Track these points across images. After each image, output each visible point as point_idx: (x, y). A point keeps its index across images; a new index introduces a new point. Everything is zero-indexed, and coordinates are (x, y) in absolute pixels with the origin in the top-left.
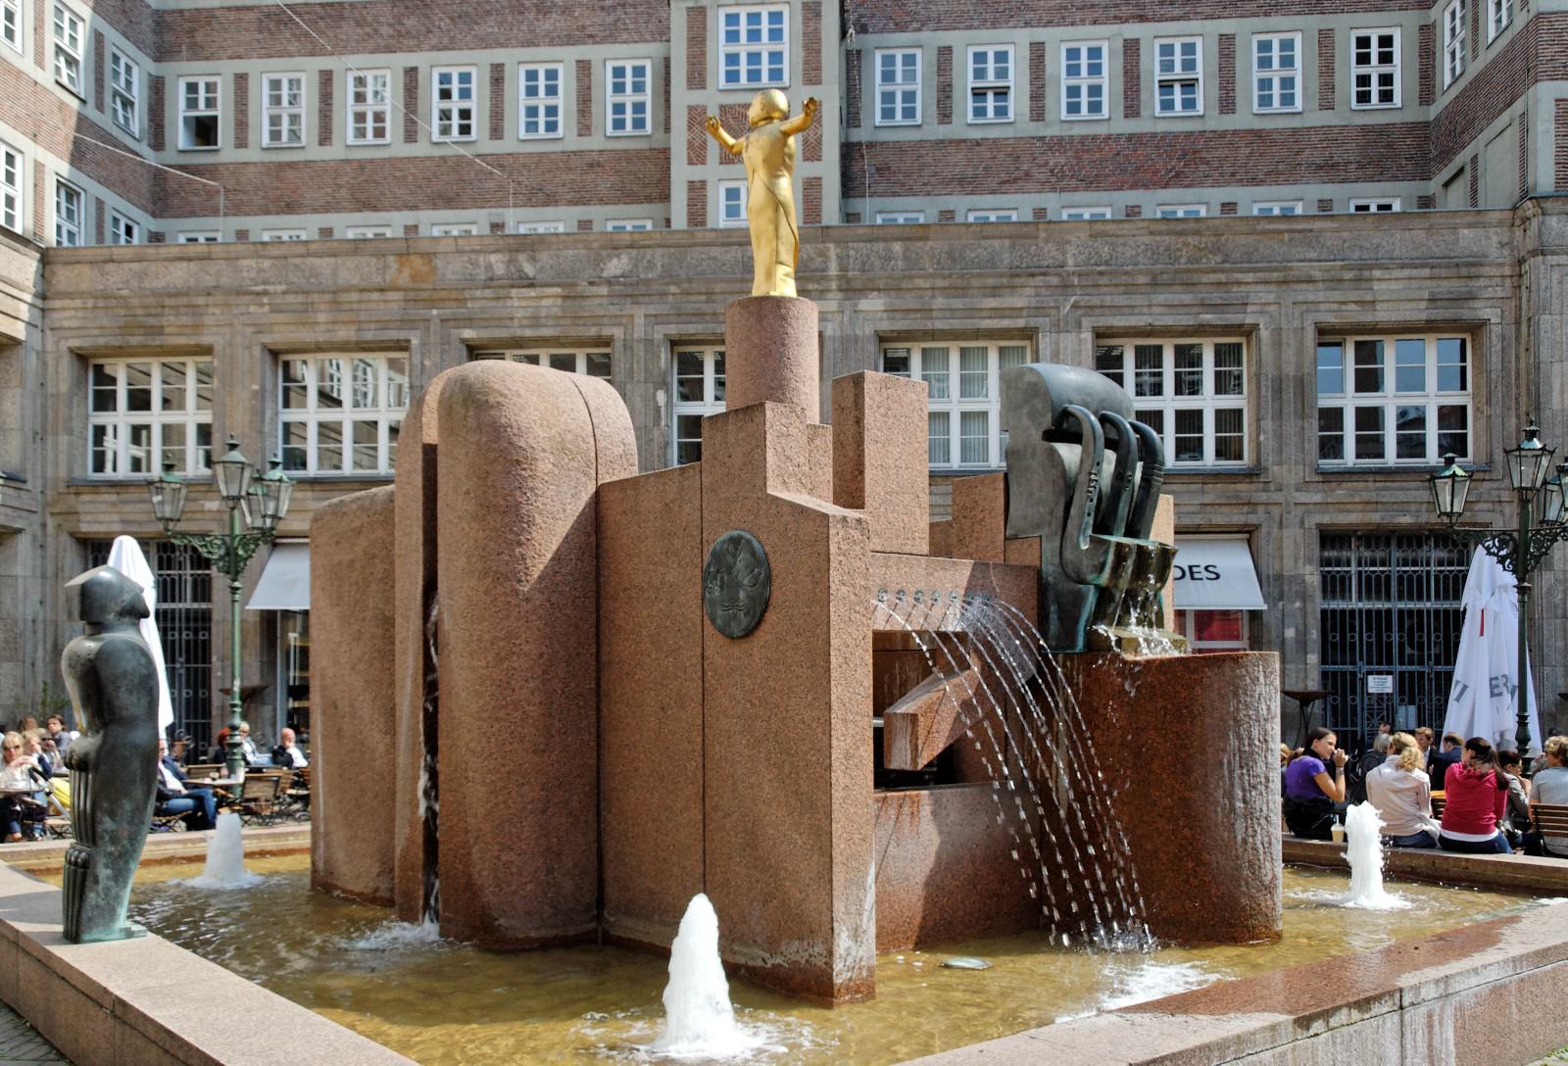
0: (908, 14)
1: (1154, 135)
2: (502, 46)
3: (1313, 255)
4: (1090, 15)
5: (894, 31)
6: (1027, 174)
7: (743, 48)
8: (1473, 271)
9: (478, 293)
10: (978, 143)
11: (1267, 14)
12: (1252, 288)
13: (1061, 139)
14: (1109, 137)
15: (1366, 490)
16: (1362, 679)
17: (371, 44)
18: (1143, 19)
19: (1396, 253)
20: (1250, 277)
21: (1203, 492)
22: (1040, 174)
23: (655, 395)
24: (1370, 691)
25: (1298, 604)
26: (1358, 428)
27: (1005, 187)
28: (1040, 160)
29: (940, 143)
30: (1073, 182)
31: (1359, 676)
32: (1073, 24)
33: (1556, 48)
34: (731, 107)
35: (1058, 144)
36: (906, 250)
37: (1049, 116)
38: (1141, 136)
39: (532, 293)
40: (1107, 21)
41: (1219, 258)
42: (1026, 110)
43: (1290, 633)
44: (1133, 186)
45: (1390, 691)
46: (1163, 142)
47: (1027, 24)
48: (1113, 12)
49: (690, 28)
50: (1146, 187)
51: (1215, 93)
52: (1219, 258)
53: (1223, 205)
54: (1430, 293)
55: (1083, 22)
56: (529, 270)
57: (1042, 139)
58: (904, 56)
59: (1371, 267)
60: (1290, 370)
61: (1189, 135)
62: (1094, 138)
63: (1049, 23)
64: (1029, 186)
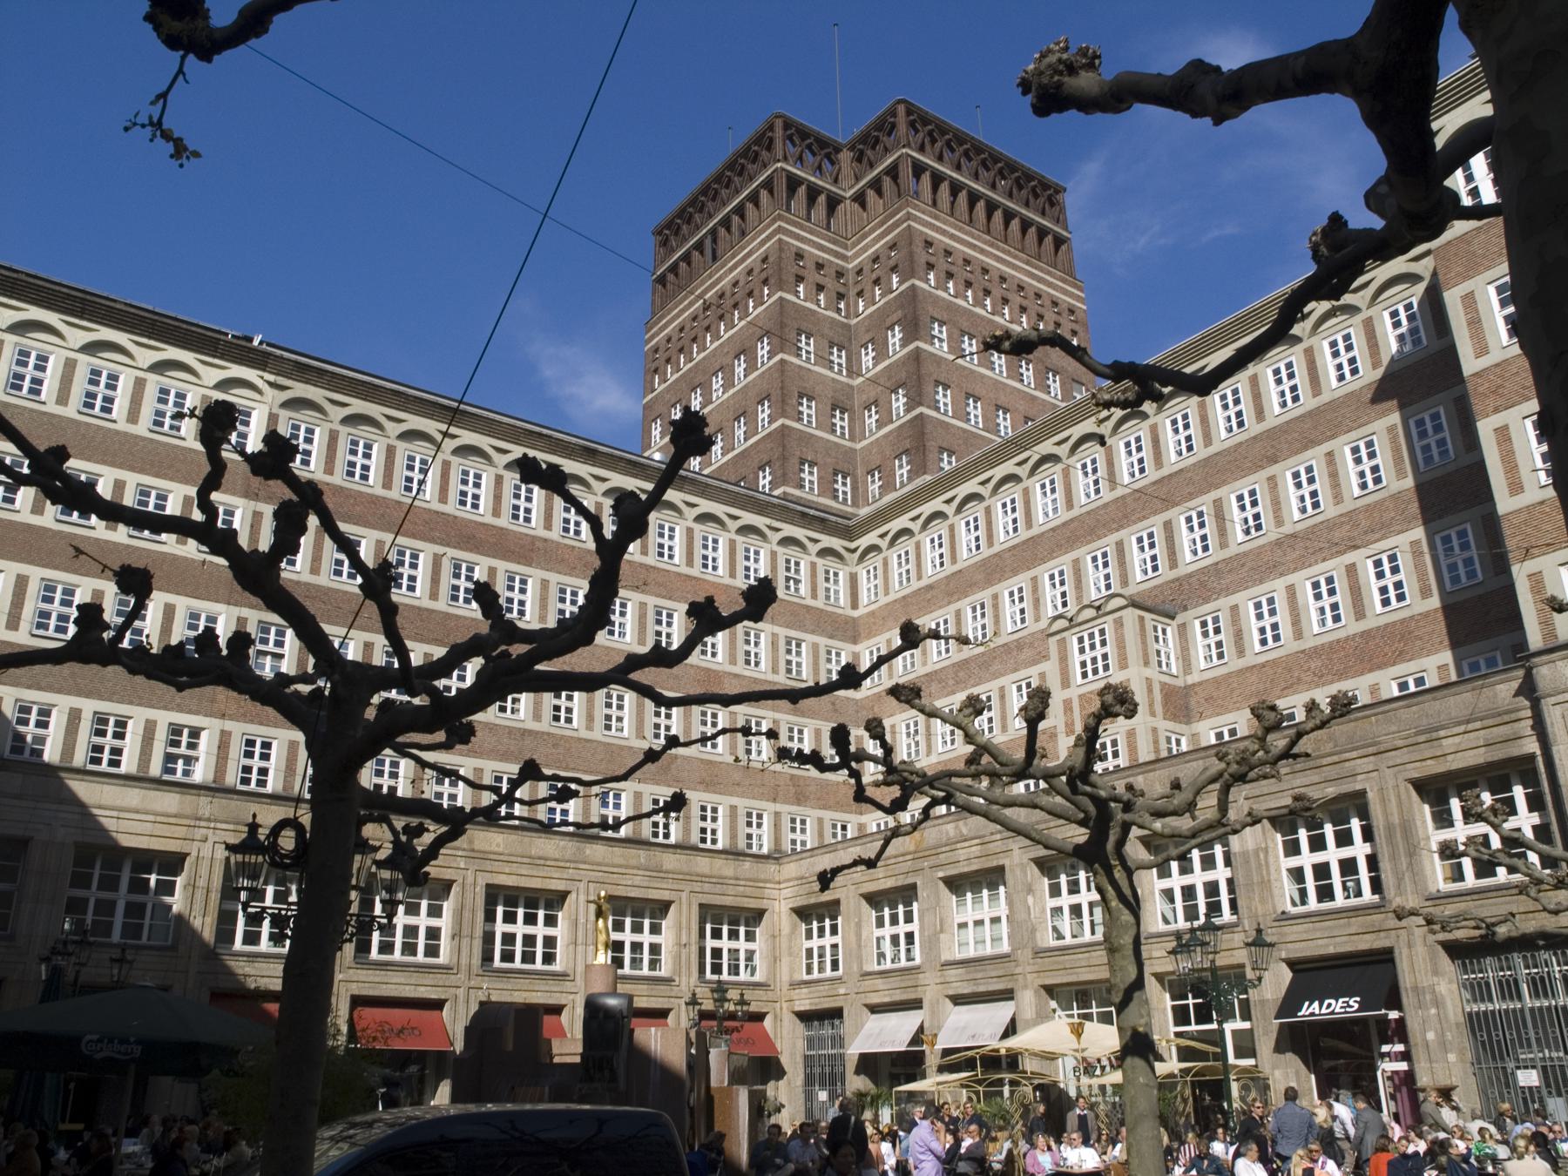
0: (1209, 590)
1: (1378, 628)
2: (1003, 675)
3: (1394, 728)
4: (1320, 556)
5: (1202, 604)
6: (1299, 679)
7: (1098, 653)
8: (1513, 716)
9: (944, 849)
10: (1263, 665)
11: (1440, 517)
12: (1359, 761)
13: (1316, 648)
14: (1347, 638)
15: (1357, 923)
16: (1513, 1073)
17: (945, 692)
18: (1356, 547)
19: (1453, 715)
20: (1354, 754)
21: (1349, 925)
22: (1307, 677)
23: (1026, 901)
24: (1522, 1084)
25: (1433, 1011)
26: (1316, 880)
27: (1285, 692)
28: (1305, 668)
29: (1241, 672)
30: (1330, 677)
31: (1509, 1071)
32: (1310, 566)
33: (1518, 538)
34: (1084, 695)
35: (1315, 652)
36: (1145, 779)
37: (1306, 634)
38: (1370, 631)
39: (966, 844)
40: (1332, 556)
41: (1331, 745)
42: (1291, 635)
43: (1431, 1036)
44: (1371, 670)
45: (1537, 1084)
46: (1386, 631)
47: (1282, 575)
48: (1334, 550)
49: (1060, 653)
50: (1379, 667)
51: (1416, 586)
52: (1331, 745)
53: (1439, 667)
54: (1485, 739)
55: (1316, 562)
56: (965, 831)
57: (1303, 652)
58: (534, 962)
59: (1437, 729)
60: (1396, 819)
61: (1403, 621)
62: (1338, 641)
63: (1295, 570)
64: (1301, 687)
